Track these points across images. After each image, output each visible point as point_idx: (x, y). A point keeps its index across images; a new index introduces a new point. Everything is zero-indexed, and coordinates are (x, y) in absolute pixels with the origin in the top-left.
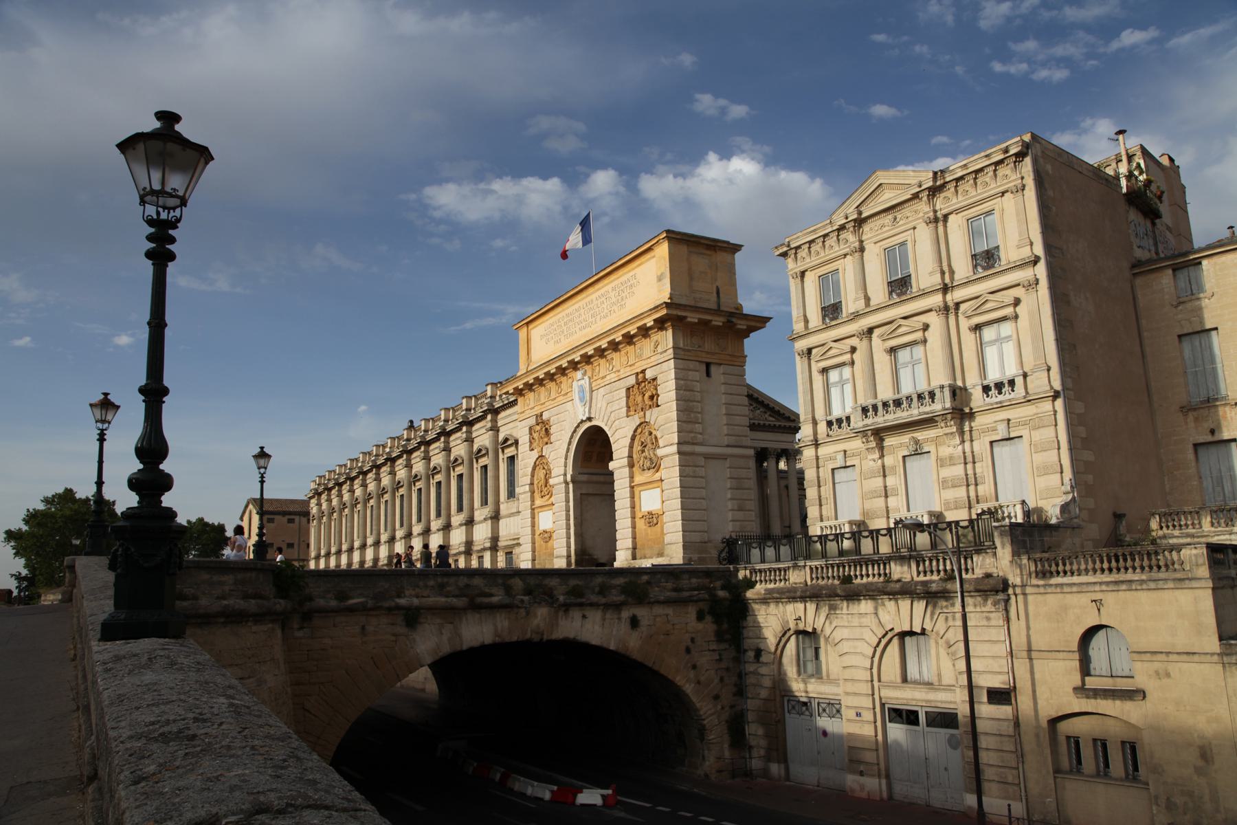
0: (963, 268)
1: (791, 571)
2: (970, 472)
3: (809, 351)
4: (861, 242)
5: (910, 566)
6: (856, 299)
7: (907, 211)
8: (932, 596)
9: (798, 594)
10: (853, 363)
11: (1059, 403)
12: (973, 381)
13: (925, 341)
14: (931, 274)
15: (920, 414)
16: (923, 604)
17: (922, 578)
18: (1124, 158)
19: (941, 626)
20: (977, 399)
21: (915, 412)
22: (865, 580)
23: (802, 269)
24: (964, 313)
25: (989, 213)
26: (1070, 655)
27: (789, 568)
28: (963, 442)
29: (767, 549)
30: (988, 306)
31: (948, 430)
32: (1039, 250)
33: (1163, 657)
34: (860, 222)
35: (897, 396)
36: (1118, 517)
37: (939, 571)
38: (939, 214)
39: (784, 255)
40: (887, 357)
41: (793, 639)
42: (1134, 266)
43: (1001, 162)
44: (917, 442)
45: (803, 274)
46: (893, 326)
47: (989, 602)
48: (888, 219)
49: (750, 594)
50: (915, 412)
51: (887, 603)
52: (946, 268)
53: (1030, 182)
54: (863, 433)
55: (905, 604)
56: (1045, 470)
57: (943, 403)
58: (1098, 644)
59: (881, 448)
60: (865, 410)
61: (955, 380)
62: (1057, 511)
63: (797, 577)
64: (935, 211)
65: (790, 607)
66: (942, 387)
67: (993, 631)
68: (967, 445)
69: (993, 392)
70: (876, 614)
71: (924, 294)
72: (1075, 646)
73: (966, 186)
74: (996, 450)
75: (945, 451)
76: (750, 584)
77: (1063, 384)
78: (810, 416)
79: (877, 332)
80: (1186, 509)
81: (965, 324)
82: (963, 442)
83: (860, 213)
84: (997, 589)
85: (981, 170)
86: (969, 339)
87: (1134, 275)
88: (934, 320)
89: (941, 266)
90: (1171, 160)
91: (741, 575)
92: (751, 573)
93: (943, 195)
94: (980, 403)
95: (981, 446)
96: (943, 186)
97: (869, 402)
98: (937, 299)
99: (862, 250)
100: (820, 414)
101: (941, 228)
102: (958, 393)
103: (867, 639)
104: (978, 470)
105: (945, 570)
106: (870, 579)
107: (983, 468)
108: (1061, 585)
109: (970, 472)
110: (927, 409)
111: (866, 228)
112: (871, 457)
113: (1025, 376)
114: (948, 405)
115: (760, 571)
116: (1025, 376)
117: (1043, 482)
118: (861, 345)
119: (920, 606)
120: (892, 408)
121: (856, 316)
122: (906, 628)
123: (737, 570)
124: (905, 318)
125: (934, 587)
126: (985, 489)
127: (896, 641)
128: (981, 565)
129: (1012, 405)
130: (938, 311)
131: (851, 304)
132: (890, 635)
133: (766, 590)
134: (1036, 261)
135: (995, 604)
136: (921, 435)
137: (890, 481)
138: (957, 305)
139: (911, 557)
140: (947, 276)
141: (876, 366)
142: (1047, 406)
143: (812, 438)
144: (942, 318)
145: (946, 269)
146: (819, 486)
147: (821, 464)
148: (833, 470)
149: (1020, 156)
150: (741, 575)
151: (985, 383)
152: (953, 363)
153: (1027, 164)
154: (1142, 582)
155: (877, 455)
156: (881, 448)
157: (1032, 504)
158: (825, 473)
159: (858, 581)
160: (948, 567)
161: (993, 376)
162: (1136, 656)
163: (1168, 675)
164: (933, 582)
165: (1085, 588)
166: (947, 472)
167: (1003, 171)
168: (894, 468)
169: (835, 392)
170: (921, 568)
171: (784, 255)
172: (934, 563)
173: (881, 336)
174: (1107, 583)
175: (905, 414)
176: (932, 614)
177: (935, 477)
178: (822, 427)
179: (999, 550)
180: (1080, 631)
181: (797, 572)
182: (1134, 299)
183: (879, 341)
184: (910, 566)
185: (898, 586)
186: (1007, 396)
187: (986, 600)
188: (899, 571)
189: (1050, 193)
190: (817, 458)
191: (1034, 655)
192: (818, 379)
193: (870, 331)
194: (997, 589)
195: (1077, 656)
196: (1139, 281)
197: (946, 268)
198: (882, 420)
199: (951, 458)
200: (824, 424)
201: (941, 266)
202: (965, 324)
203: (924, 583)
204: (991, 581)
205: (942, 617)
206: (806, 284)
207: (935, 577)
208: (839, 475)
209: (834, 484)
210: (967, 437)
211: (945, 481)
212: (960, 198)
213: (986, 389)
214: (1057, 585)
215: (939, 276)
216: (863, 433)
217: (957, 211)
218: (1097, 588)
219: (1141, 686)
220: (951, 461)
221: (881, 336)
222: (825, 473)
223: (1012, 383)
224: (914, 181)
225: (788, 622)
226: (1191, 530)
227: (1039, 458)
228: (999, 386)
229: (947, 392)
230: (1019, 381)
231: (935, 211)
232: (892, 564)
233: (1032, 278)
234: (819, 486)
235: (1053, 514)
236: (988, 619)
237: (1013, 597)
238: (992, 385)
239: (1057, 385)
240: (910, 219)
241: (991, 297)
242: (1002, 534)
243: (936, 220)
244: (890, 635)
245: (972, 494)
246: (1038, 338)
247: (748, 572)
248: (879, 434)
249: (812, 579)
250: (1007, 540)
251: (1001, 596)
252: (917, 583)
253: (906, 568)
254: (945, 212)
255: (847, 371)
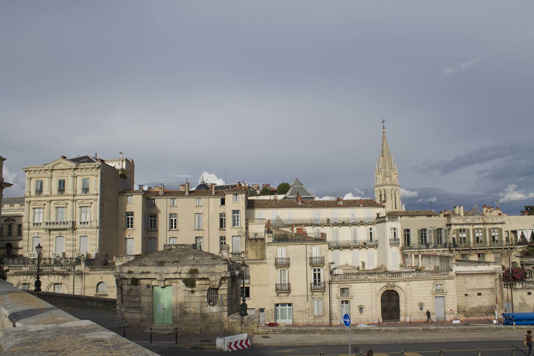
0: (79, 191)
1: (23, 267)
2: (74, 243)
3: (30, 202)
4: (52, 175)
5: (59, 268)
6: (48, 191)
7: (67, 171)
8: (64, 275)
9: (26, 273)
10: (44, 208)
11: (98, 230)
12: (78, 220)
13: (66, 207)
14: (71, 190)
15: (63, 227)
16: (62, 276)
17: (62, 270)
18: (121, 160)
19: (66, 282)
20: (78, 225)
21: (62, 226)
22: (46, 270)
23: (31, 177)
24: (78, 203)
25: (88, 179)
26: (95, 288)
27: (22, 266)
28: (73, 235)
29: (15, 261)
30: (84, 202)
31: (70, 232)
32: (99, 192)
33: (112, 288)
34: (53, 170)
35: (57, 221)
36: (107, 256)
37: (66, 269)
38: (75, 175)
39: (26, 171)
40: (55, 209)
41: (21, 285)
42: (119, 193)
43: (93, 168)
44: (60, 233)
45: (31, 178)
46: (58, 201)
47: (78, 276)
48: (61, 171)
49: (8, 273)
50: (62, 226)
51: (52, 276)
52: (75, 190)
53: (99, 175)
54: (46, 229)
55: (57, 277)
56: (92, 245)
57: (70, 226)
58: (101, 286)
59: (50, 233)
60: (47, 223)
61: (73, 219)
62: (94, 255)
63: (25, 269)
64: (74, 174)
65: (22, 277)
66: (70, 221)
67: (78, 283)
68: (74, 236)
69: (83, 224)
70: (48, 279)
71: (68, 195)
72: (96, 286)
73: (84, 170)
74: (81, 238)
75: (68, 237)
76: (8, 271)
77: (99, 225)
78: (28, 221)
79: (52, 202)
80: (121, 255)
81: (78, 206)
82: (73, 235)
83: (53, 168)
84: (81, 274)
85: (88, 168)
86: (78, 210)
87: (119, 195)
88: (70, 203)
89: (74, 189)
90: (132, 160)
91: (5, 268)
92: (9, 267)
93: (77, 171)
94: (79, 226)
95: (78, 237)
96: (78, 168)
97: (48, 221)
98: (72, 198)
99: (52, 178)
100: (31, 220)
101: (75, 179)
102: (74, 223)
103: (45, 285)
104: (76, 243)
105: (68, 269)
106: (48, 270)
107: (77, 242)
108: (95, 273)
109: (74, 243)
110: (65, 226)
111: (54, 172)
112: (46, 235)
113: (91, 222)
114: (71, 226)
115: (12, 267)
116: (91, 222)
117: (92, 247)
118: (47, 205)
119: (61, 277)
120: (55, 224)
121: (47, 196)
122: (57, 282)
123: (3, 266)
124: (62, 200)
125: (65, 273)
126: (77, 248)
127: (53, 285)
128: (77, 268)
129: (87, 228)
130: (71, 201)
131: (46, 191)
132: (51, 284)
133: (14, 272)
134: (98, 195)
135: (79, 277)
136: (62, 232)
137: (51, 243)
138: (76, 200)
139: (60, 265)
140: (75, 192)
141: (51, 211)
142: (95, 230)
143: (28, 227)
144: (72, 203)
145: (75, 190)
146: (28, 241)
147: (30, 235)
148: (33, 237)
149: (98, 168)
150: (5, 268)
151: (81, 221)
152: (73, 215)
153: (100, 169)
154: (111, 273)
155: (48, 235)
156: (50, 233)
157: (88, 253)
158: (31, 238)
159: (44, 270)
160: (69, 268)
161: (83, 220)
162: (107, 288)
163: (113, 291)
164: (65, 272)
165: (99, 274)
166: (68, 242)
167: (93, 170)
168: (53, 239)
169: (37, 215)
170: (62, 268)
171: (26, 171)
172: (65, 267)
173: (54, 203)
174: (104, 273)
175: (59, 226)
176: (64, 279)
177: (64, 243)
178: (31, 225)
179: (82, 265)
180: (97, 283)
181: (25, 268)
182: (118, 201)
183: (53, 205)
184: (59, 268)
185: (56, 272)
186: (86, 225)
187: (77, 276)
188: (56, 269)
189: (103, 178)
190: (29, 233)
191: (85, 288)
192: (32, 211)
193: (51, 201)
194: (81, 274)
195: (96, 288)
196: (119, 197)
197: (75, 190)
198: (52, 227)
199: (70, 239)
200: (32, 224)
201: (74, 189)
202: (78, 206)
203: (63, 272)
204: (79, 272)
205: (66, 280)
206: (31, 182)
207: (65, 270)
208: (35, 239)
209: (33, 241)
210: (74, 234)
211: (67, 244)
212: (82, 173)
213: (81, 223)
214: (94, 273)
215: (73, 192)
216: (46, 229)
217: (80, 176)
218: (102, 274)
219: (107, 294)
220: (69, 240)
221: (54, 203)
222: (31, 238)
223: (87, 223)
224: (71, 165)
225: (20, 281)
226: (121, 260)
227: (91, 242)
228: (84, 223)
229: (71, 223)
230: (89, 223)
231: (74, 174)
232: (54, 267)
233: (96, 199)
234: (28, 241)
235: (93, 256)
236: (77, 280)
237: (84, 276)
238: (83, 222)
239: (98, 225)
240: (67, 174)
241: (85, 200)
242: (83, 261)
243: (74, 177)
244: (51, 284)
245: (74, 249)
246: (95, 213)
247: (8, 267)
248: (50, 230)
249: (30, 270)
250: (84, 263)
251: (81, 275)
252: (61, 272)
253: (58, 268)
254: (77, 175)
255: (41, 210)
